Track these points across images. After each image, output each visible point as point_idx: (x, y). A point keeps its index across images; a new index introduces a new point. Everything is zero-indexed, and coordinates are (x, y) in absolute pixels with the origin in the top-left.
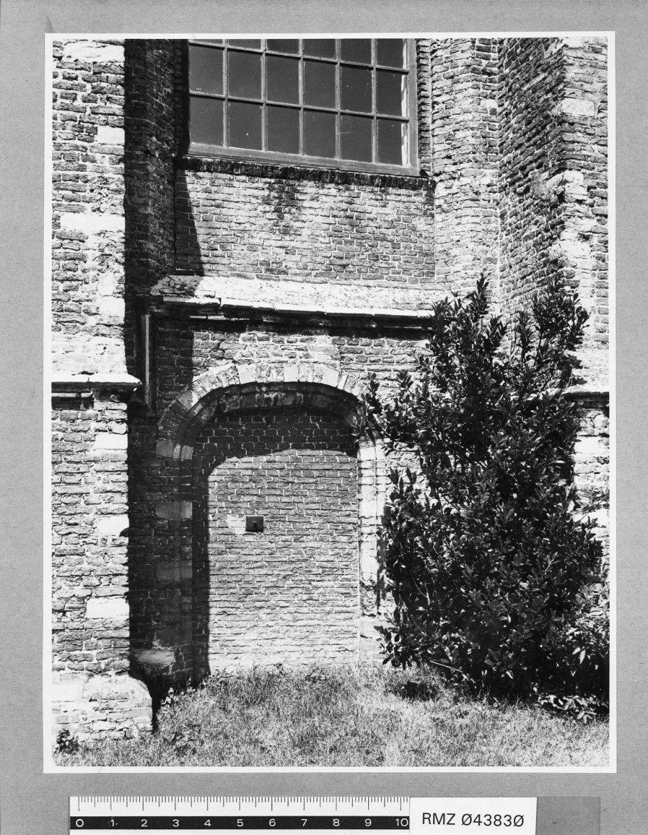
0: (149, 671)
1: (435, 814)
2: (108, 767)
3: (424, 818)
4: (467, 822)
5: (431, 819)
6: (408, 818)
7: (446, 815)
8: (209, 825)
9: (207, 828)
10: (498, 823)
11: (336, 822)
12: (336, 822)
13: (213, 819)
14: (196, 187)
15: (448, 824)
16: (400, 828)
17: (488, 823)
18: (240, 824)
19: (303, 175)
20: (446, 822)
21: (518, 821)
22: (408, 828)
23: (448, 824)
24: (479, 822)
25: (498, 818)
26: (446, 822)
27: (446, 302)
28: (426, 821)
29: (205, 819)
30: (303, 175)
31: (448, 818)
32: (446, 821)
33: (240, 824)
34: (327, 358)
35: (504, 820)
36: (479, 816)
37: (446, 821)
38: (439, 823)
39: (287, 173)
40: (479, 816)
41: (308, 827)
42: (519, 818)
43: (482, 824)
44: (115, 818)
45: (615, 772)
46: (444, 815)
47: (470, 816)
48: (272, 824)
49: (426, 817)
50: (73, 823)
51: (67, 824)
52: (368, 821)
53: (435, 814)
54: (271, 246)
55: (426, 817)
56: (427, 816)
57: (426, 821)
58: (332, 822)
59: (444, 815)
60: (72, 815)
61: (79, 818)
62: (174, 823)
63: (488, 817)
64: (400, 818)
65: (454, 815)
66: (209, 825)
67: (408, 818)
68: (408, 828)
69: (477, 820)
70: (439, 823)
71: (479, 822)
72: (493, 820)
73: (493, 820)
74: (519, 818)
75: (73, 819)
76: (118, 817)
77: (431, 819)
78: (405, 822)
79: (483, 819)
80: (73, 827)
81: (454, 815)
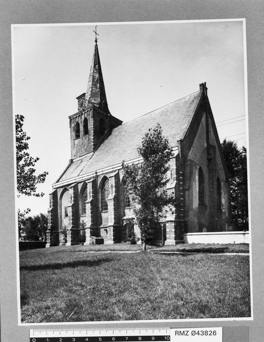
1: (180, 331)
3: (176, 333)
4: (194, 334)
5: (179, 333)
6: (169, 336)
7: (185, 332)
10: (206, 334)
11: (140, 338)
12: (140, 338)
14: (125, 210)
15: (186, 335)
16: (166, 340)
17: (202, 334)
18: (100, 340)
19: (131, 208)
21: (215, 333)
22: (169, 340)
23: (186, 335)
24: (199, 334)
25: (206, 332)
26: (185, 334)
28: (177, 334)
30: (131, 208)
31: (186, 333)
33: (100, 340)
34: (173, 149)
35: (209, 333)
36: (198, 331)
38: (182, 335)
39: (130, 209)
40: (198, 331)
44: (49, 338)
46: (184, 331)
47: (195, 332)
49: (176, 333)
52: (153, 338)
53: (180, 331)
54: (129, 214)
56: (177, 332)
57: (177, 334)
58: (138, 338)
59: (184, 331)
60: (31, 337)
61: (34, 338)
62: (73, 340)
63: (202, 332)
64: (166, 336)
65: (188, 331)
67: (169, 336)
68: (169, 340)
69: (198, 333)
70: (182, 335)
71: (199, 334)
72: (204, 333)
73: (204, 333)
77: (179, 333)
78: (168, 338)
79: (200, 333)
81: (188, 331)
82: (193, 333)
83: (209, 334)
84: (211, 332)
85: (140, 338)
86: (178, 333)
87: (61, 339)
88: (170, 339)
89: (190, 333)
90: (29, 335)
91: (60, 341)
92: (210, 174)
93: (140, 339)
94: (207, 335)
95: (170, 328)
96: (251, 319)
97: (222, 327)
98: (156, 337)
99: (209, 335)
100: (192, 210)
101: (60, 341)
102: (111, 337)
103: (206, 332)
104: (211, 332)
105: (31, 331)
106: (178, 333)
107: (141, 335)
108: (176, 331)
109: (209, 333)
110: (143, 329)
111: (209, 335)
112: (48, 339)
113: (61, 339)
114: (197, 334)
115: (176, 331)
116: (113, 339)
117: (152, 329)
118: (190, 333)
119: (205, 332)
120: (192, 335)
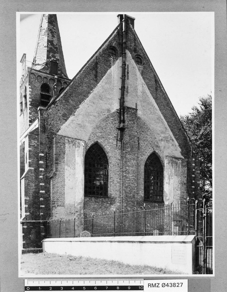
0: (149, 270)
1: (152, 284)
2: (104, 275)
3: (149, 285)
4: (164, 286)
5: (151, 285)
6: (143, 286)
7: (156, 284)
8: (73, 289)
9: (73, 290)
10: (174, 286)
11: (118, 288)
12: (118, 288)
13: (75, 287)
15: (157, 287)
17: (171, 286)
20: (156, 286)
22: (143, 290)
23: (157, 287)
24: (168, 286)
25: (174, 284)
26: (156, 286)
27: (30, 120)
28: (149, 286)
29: (72, 287)
31: (157, 285)
32: (156, 286)
35: (177, 285)
36: (168, 284)
37: (156, 286)
38: (154, 287)
40: (168, 284)
41: (108, 289)
42: (163, 286)
43: (169, 287)
44: (40, 287)
45: (214, 13)
46: (155, 284)
47: (165, 284)
48: (96, 288)
49: (149, 285)
50: (26, 288)
51: (24, 288)
53: (152, 284)
55: (149, 285)
56: (149, 285)
57: (149, 286)
59: (155, 284)
60: (26, 285)
62: (61, 288)
63: (171, 284)
64: (140, 286)
65: (159, 284)
66: (73, 289)
67: (143, 286)
68: (143, 290)
69: (167, 285)
70: (154, 287)
71: (168, 286)
72: (173, 285)
73: (173, 285)
74: (163, 286)
75: (26, 287)
76: (42, 286)
77: (151, 285)
78: (142, 288)
79: (169, 285)
80: (26, 290)
81: (182, 283)
82: (164, 285)
83: (176, 286)
84: (178, 284)
85: (118, 287)
86: (150, 285)
87: (51, 288)
88: (143, 289)
89: (160, 285)
90: (24, 284)
91: (50, 289)
92: (48, 187)
93: (118, 288)
94: (172, 286)
95: (143, 279)
96: (213, 275)
97: (187, 280)
98: (132, 287)
99: (177, 286)
100: (63, 206)
101: (50, 289)
102: (38, 287)
103: (174, 284)
104: (178, 284)
105: (26, 281)
106: (150, 285)
107: (63, 286)
108: (148, 284)
109: (177, 285)
110: (104, 280)
111: (177, 286)
112: (40, 288)
113: (51, 288)
114: (166, 286)
115: (148, 284)
116: (95, 288)
117: (55, 281)
118: (160, 285)
119: (173, 284)
120: (162, 286)
